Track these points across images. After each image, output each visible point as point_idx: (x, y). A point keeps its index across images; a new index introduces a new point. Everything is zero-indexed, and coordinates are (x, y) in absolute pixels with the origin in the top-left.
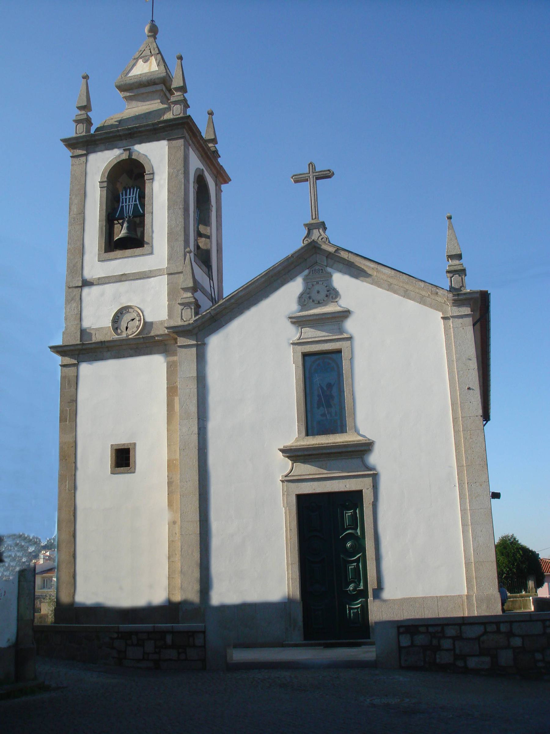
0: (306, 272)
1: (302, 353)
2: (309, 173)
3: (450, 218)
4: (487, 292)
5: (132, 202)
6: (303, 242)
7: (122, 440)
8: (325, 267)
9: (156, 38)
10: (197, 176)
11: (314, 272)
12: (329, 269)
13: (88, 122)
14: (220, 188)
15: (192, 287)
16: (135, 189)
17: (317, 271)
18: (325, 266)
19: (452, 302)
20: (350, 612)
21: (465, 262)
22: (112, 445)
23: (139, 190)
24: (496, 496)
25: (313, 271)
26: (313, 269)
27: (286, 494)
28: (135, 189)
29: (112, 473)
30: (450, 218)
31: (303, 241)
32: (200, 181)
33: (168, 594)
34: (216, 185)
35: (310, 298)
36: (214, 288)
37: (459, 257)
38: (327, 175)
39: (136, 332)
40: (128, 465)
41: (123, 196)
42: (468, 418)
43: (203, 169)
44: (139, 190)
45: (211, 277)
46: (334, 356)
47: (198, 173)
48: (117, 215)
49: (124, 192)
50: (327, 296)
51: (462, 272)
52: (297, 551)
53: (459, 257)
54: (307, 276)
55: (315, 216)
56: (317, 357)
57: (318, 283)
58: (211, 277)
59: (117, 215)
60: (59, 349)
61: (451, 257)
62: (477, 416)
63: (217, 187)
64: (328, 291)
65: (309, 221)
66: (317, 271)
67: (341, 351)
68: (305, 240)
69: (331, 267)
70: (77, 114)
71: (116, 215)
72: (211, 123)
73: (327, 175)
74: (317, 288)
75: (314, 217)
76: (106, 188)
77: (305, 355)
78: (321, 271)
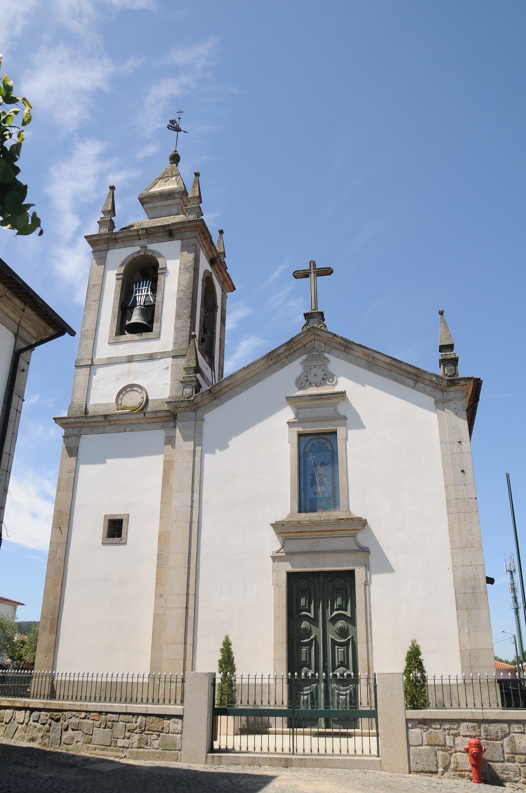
0: (304, 357)
1: (297, 431)
2: (310, 270)
3: (441, 313)
4: (479, 379)
5: (144, 293)
6: (303, 330)
7: (116, 512)
8: (323, 353)
9: (178, 166)
10: (206, 277)
11: (312, 356)
12: (326, 355)
13: (112, 224)
14: (226, 295)
15: (195, 367)
16: (148, 282)
17: (315, 356)
18: (323, 351)
19: (278, 562)
20: (338, 699)
21: (457, 352)
22: (105, 516)
23: (151, 282)
24: (490, 581)
25: (311, 356)
26: (312, 354)
27: (275, 570)
28: (148, 282)
29: (103, 544)
30: (441, 313)
31: (303, 328)
32: (208, 281)
33: (454, 578)
34: (223, 290)
35: (307, 380)
36: (215, 377)
37: (451, 347)
38: (328, 272)
39: (139, 407)
40: (120, 536)
41: (136, 287)
42: (463, 500)
43: (211, 272)
44: (151, 282)
45: (213, 369)
46: (328, 437)
47: (207, 274)
48: (130, 304)
49: (138, 283)
50: (324, 379)
51: (455, 361)
52: (285, 631)
53: (451, 347)
54: (305, 361)
55: (314, 307)
56: (311, 437)
57: (315, 367)
58: (213, 369)
59: (130, 304)
60: (64, 421)
61: (442, 348)
62: (471, 498)
63: (223, 292)
64: (325, 375)
65: (308, 310)
66: (315, 356)
67: (337, 432)
68: (305, 327)
69: (329, 353)
70: (101, 217)
71: (129, 304)
72: (221, 238)
73: (328, 272)
74: (314, 371)
75: (314, 308)
76: (121, 280)
77: (300, 435)
78: (318, 356)
